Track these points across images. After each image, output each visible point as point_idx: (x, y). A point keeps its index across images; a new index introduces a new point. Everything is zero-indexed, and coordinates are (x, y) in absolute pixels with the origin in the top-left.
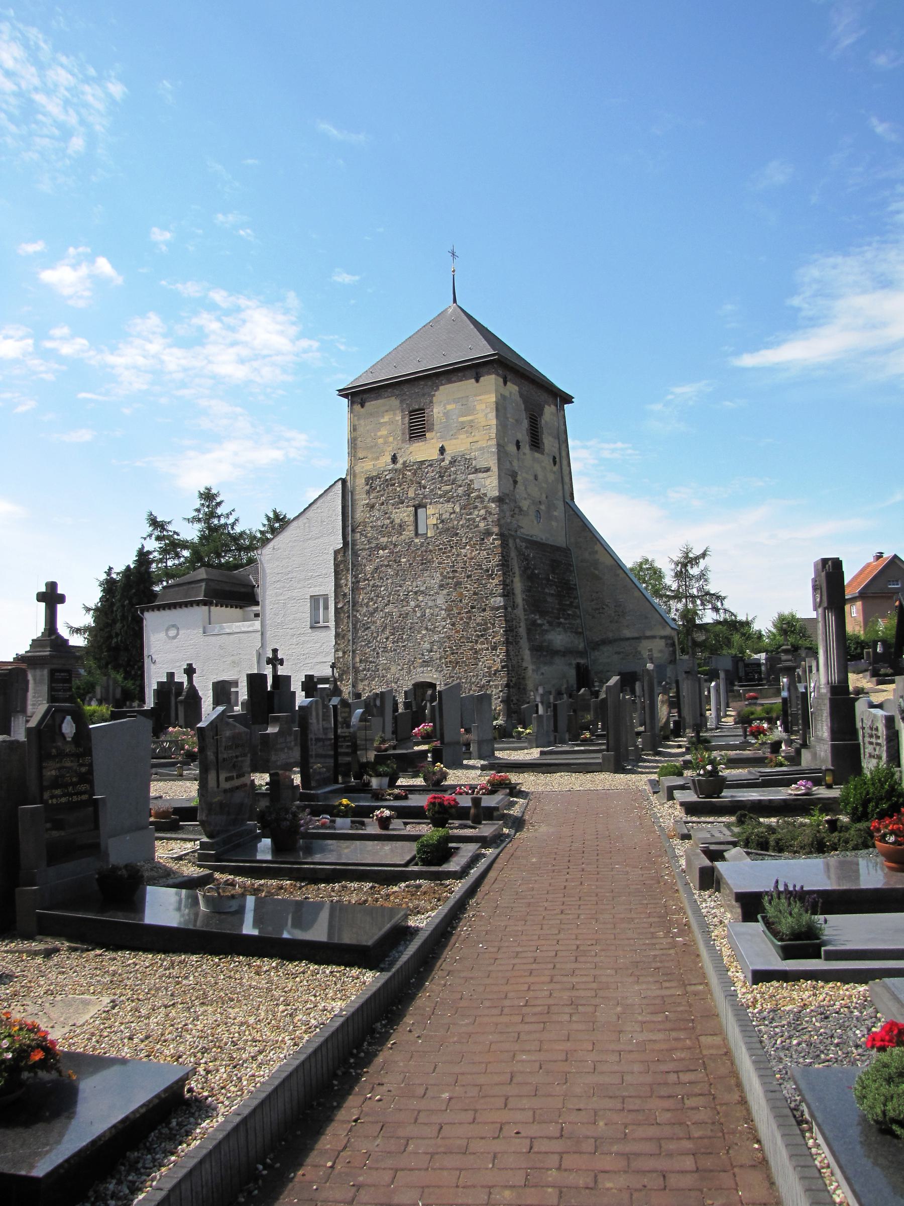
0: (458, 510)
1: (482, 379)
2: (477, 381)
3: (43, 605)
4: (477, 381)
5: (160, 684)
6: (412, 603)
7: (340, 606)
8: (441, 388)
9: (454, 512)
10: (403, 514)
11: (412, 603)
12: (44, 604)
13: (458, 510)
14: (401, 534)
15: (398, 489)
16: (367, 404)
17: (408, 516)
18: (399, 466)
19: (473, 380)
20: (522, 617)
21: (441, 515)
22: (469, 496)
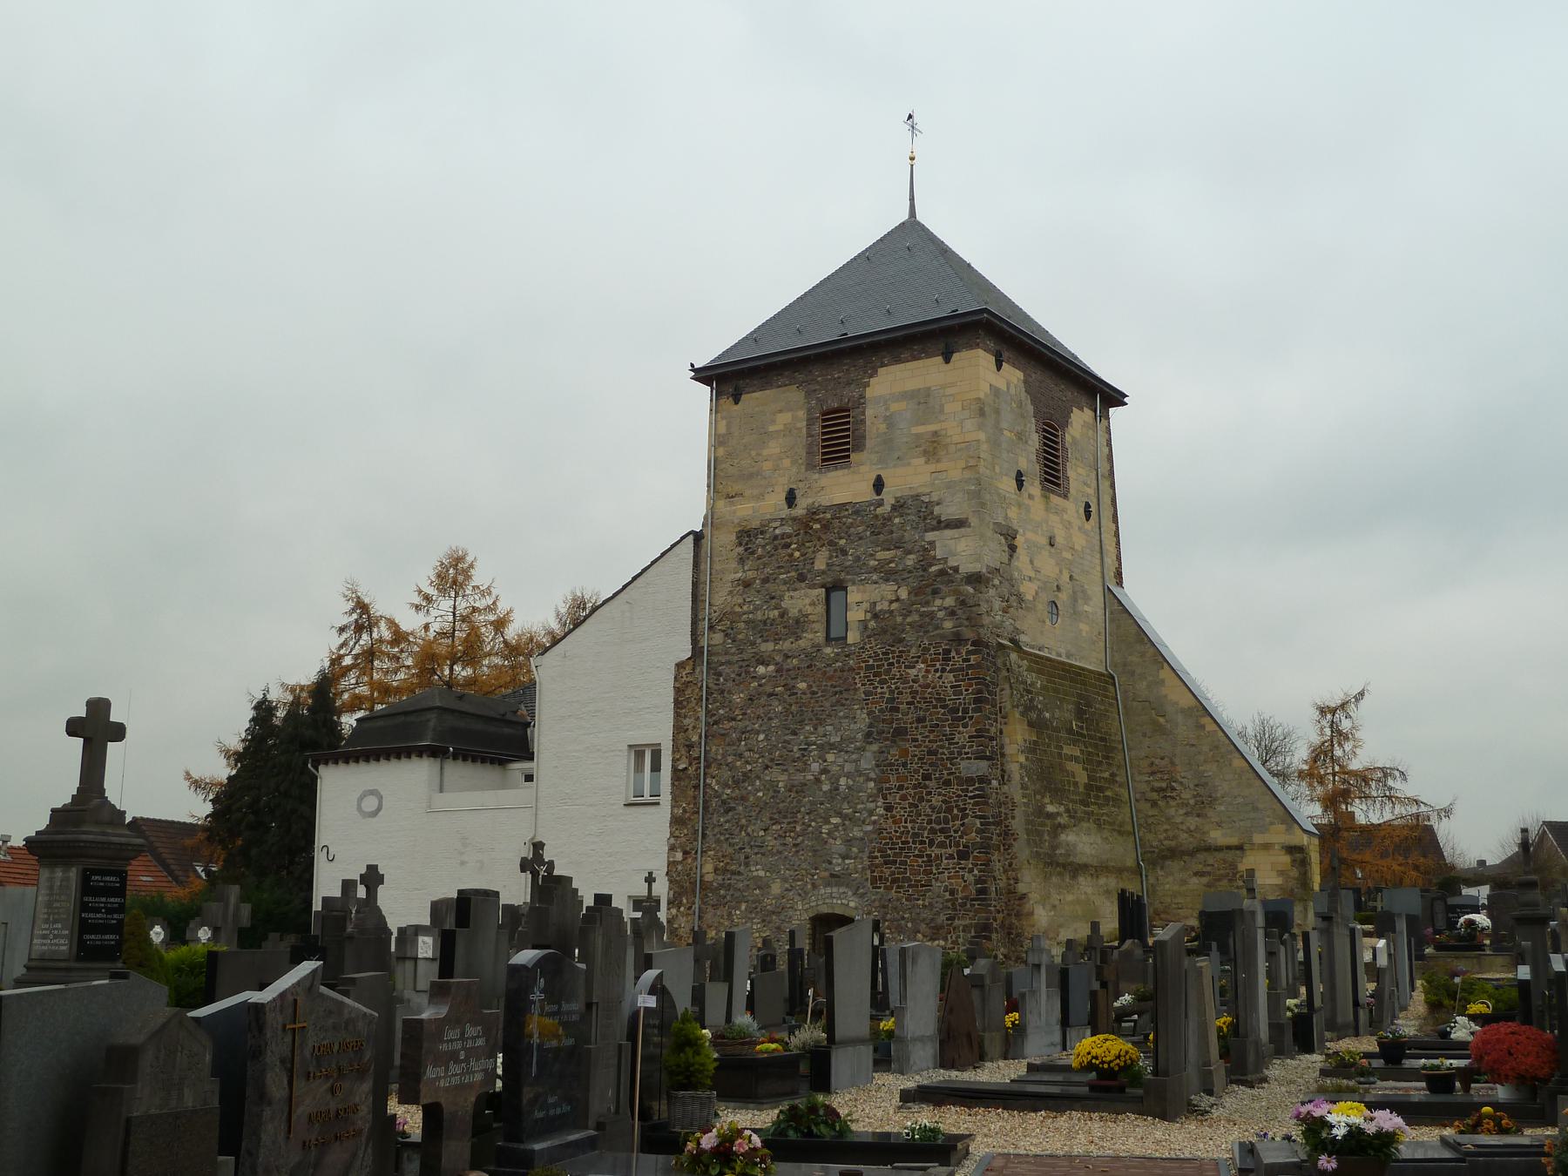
1: (956, 356)
2: (947, 361)
4: (947, 361)
6: (815, 767)
8: (881, 371)
11: (815, 767)
14: (798, 638)
15: (797, 554)
19: (940, 359)
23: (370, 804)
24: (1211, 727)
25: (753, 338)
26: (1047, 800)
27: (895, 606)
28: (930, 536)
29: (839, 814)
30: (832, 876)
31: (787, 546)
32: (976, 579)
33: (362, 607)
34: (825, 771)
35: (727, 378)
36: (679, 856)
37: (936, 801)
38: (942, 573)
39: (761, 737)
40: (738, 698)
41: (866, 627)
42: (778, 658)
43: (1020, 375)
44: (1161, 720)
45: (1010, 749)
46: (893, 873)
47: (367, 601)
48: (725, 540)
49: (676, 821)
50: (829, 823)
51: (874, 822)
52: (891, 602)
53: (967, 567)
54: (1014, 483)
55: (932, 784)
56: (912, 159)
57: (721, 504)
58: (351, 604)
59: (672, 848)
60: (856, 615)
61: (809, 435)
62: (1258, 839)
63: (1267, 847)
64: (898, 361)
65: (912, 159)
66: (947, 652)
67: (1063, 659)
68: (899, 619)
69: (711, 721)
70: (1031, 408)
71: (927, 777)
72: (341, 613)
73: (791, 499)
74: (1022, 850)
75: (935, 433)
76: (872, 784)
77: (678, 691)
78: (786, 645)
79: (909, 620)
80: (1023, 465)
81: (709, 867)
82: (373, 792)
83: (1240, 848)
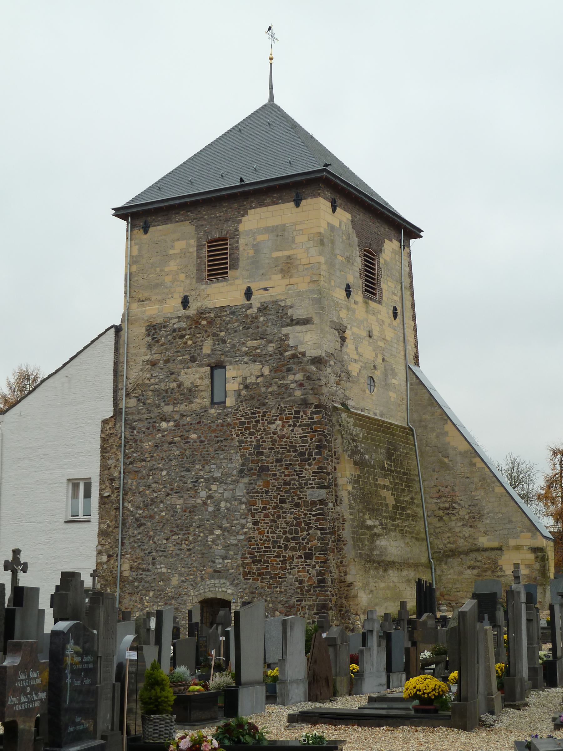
1: (303, 202)
2: (297, 205)
4: (297, 205)
8: (251, 212)
11: (203, 494)
14: (191, 402)
15: (190, 342)
19: (292, 204)
24: (480, 465)
28: (285, 330)
29: (220, 528)
34: (210, 497)
35: (139, 215)
36: (104, 558)
37: (290, 518)
38: (294, 356)
39: (164, 473)
40: (147, 445)
41: (239, 395)
42: (177, 417)
43: (348, 216)
44: (446, 460)
49: (102, 534)
55: (286, 506)
56: (271, 59)
57: (135, 306)
59: (99, 553)
65: (271, 59)
67: (378, 417)
68: (263, 389)
71: (283, 501)
73: (185, 302)
74: (349, 552)
75: (289, 257)
78: (182, 407)
79: (270, 389)
81: (126, 566)
83: (500, 549)
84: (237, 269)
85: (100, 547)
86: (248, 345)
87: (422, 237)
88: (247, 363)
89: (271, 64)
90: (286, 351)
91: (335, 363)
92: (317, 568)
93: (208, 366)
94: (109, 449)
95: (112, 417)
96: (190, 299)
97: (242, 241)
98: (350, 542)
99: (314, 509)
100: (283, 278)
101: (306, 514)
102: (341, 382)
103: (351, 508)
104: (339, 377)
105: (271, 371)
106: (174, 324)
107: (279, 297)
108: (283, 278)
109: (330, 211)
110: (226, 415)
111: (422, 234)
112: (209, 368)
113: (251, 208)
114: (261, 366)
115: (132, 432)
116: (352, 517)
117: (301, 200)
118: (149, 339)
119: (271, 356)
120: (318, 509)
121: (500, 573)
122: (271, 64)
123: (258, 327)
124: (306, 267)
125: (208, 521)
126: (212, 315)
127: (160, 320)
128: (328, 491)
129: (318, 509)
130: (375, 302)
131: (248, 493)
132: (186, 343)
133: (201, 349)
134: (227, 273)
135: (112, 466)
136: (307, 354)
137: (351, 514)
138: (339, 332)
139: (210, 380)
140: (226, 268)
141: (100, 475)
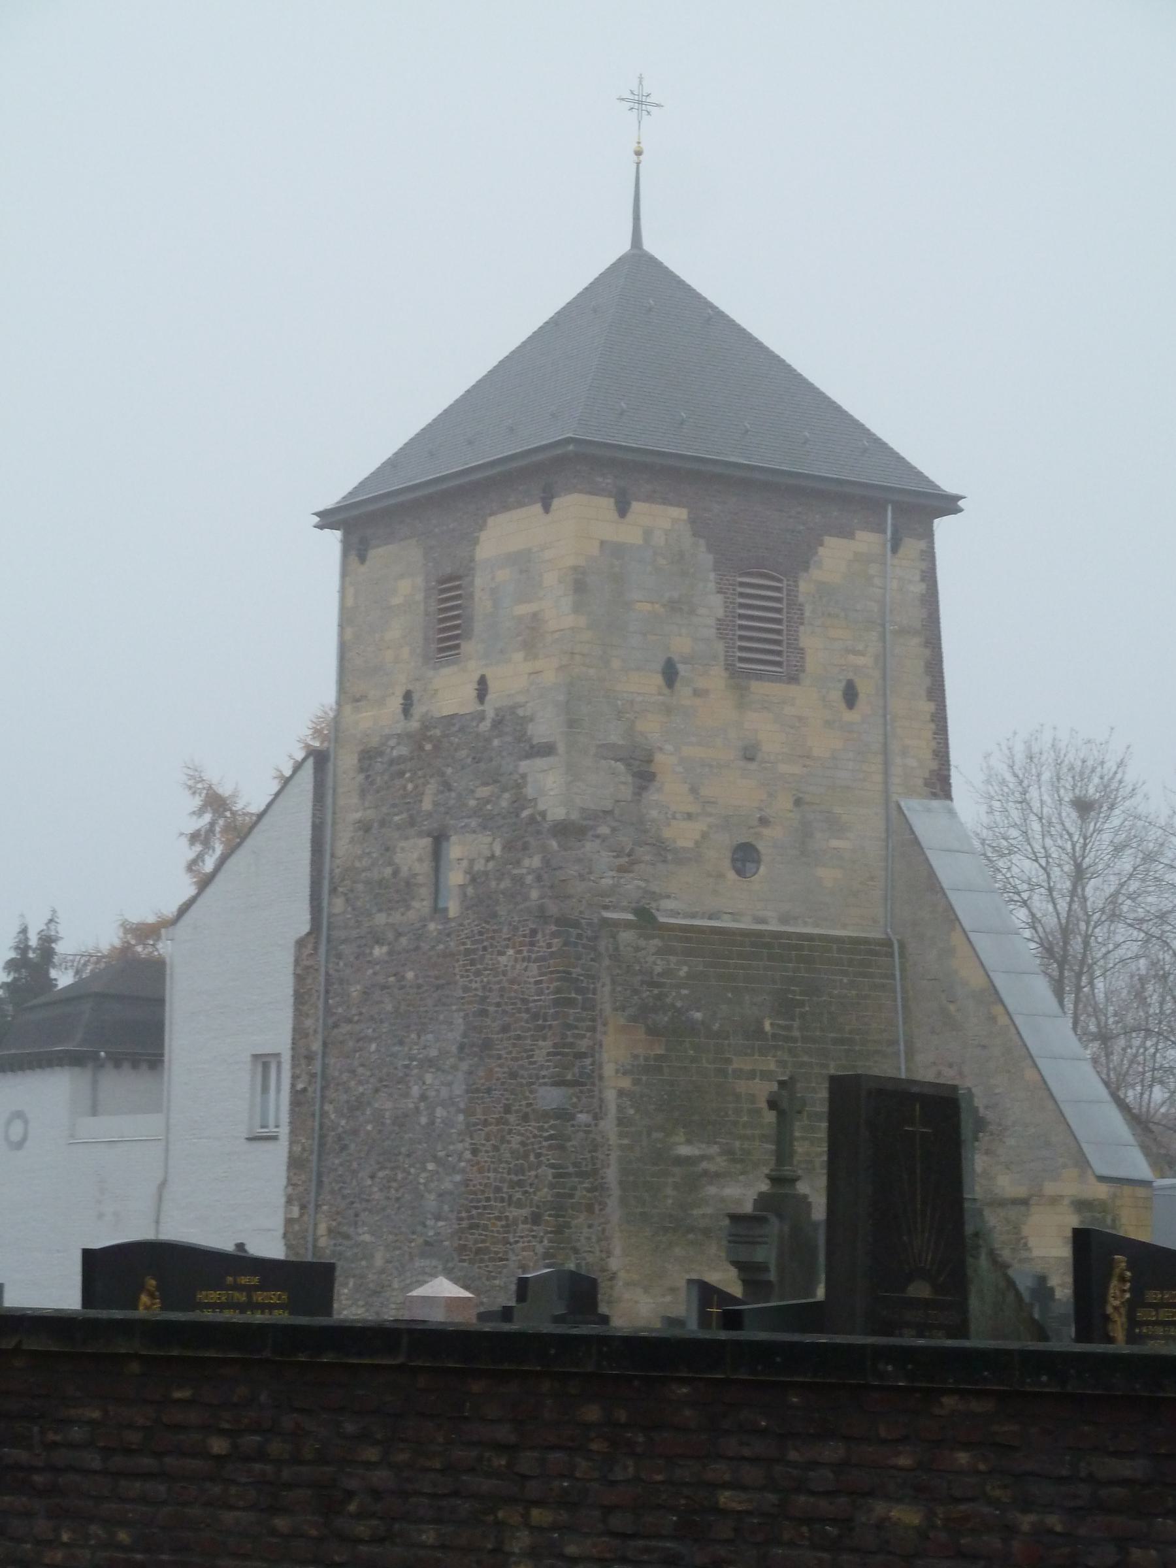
0: (498, 853)
1: (556, 503)
2: (547, 509)
3: (334, 537)
4: (547, 509)
5: (290, 1314)
6: (415, 1090)
7: (300, 1086)
8: (491, 521)
9: (493, 857)
10: (412, 854)
11: (415, 1090)
12: (338, 534)
13: (498, 853)
14: (408, 908)
15: (410, 786)
16: (373, 554)
17: (420, 860)
18: (414, 725)
19: (538, 508)
20: (613, 1139)
21: (472, 862)
22: (517, 816)
23: (17, 1129)
24: (1003, 1020)
25: (393, 464)
26: (680, 1138)
27: (491, 865)
28: (524, 766)
29: (435, 1159)
30: (427, 1243)
31: (401, 774)
32: (567, 831)
33: (215, 802)
34: (423, 1097)
35: (360, 523)
36: (295, 1212)
37: (515, 1140)
38: (532, 820)
39: (373, 1047)
40: (355, 991)
41: (465, 895)
42: (390, 936)
43: (682, 513)
44: (952, 1008)
45: (609, 1070)
46: (476, 1242)
47: (225, 790)
48: (346, 761)
49: (295, 1163)
50: (424, 1169)
51: (463, 1171)
52: (488, 860)
53: (557, 813)
54: (659, 680)
55: (512, 1118)
56: (639, 153)
57: (348, 709)
58: (197, 801)
59: (289, 1201)
60: (455, 877)
61: (427, 614)
62: (1050, 1188)
63: (1055, 1200)
64: (506, 508)
65: (639, 153)
66: (534, 932)
67: (774, 926)
68: (493, 884)
69: (331, 1021)
70: (706, 559)
71: (507, 1110)
72: (185, 814)
73: (407, 709)
74: (614, 1210)
75: (535, 616)
76: (461, 1117)
77: (299, 979)
78: (396, 917)
79: (502, 886)
80: (681, 645)
81: (322, 1228)
82: (19, 1115)
83: (1024, 1202)
84: (470, 638)
85: (290, 1189)
86: (477, 795)
87: (961, 510)
88: (474, 832)
89: (638, 164)
90: (524, 808)
91: (614, 830)
92: (546, 1242)
93: (429, 835)
94: (306, 997)
95: (309, 934)
96: (415, 697)
97: (479, 582)
98: (616, 1192)
99: (546, 1126)
100: (525, 660)
101: (535, 1136)
102: (636, 867)
103: (621, 1122)
104: (629, 855)
105: (504, 848)
106: (393, 748)
107: (521, 699)
108: (525, 660)
109: (614, 515)
110: (448, 935)
111: (961, 503)
112: (430, 839)
113: (492, 514)
114: (490, 839)
115: (338, 964)
116: (626, 1141)
117: (552, 497)
118: (361, 777)
119: (504, 818)
120: (551, 1127)
121: (1024, 1254)
122: (638, 164)
123: (491, 760)
124: (556, 636)
125: (420, 1143)
126: (438, 732)
127: (375, 741)
128: (577, 1089)
129: (551, 1127)
130: (775, 678)
131: (467, 1091)
132: (405, 788)
133: (421, 801)
134: (457, 646)
135: (311, 1031)
136: (549, 817)
137: (621, 1135)
138: (628, 765)
139: (433, 864)
140: (457, 637)
141: (293, 1049)
